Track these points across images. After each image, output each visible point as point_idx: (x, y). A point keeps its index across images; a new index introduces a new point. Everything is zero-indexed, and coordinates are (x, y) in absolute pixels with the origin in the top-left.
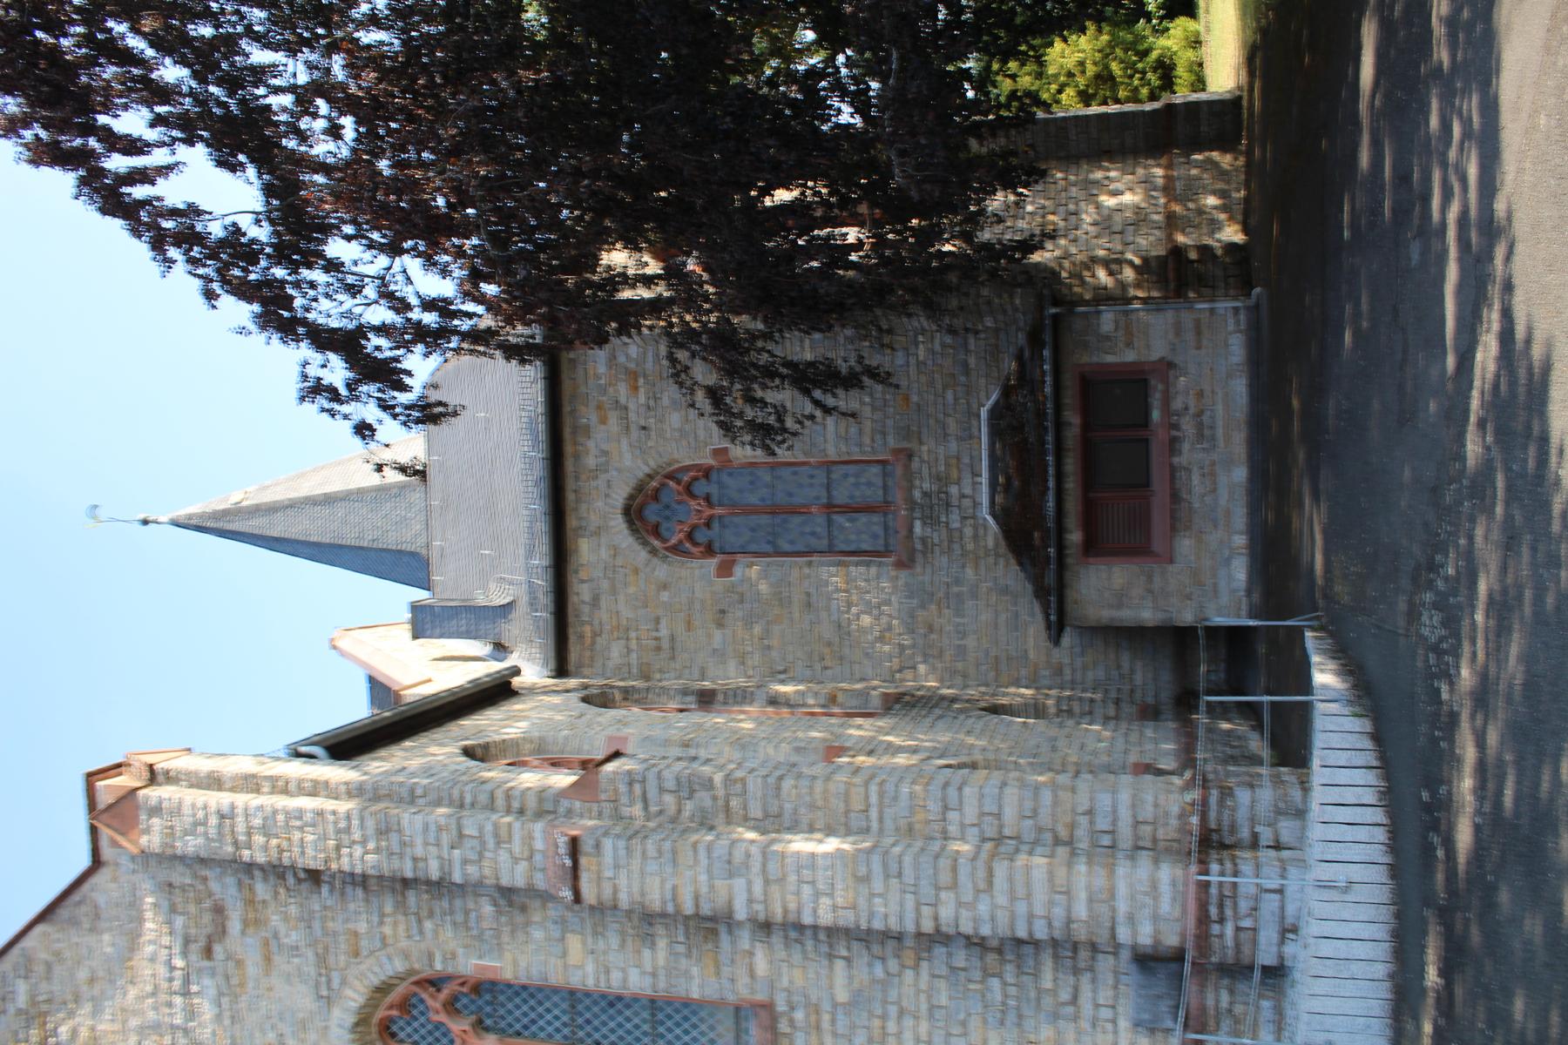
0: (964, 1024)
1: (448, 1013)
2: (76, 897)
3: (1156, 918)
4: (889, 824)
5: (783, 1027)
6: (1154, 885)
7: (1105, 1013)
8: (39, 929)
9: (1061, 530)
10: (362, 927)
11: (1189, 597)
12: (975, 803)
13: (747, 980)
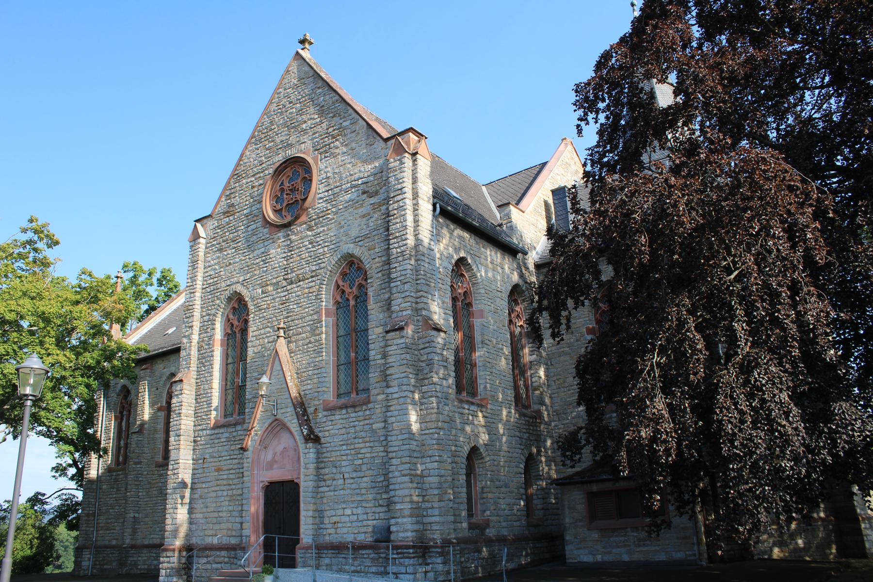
0: (370, 469)
1: (359, 285)
2: (375, 136)
3: (397, 532)
4: (424, 437)
5: (364, 407)
6: (406, 531)
7: (377, 516)
8: (365, 123)
9: (597, 481)
10: (377, 250)
11: (576, 538)
12: (432, 467)
13: (376, 393)
